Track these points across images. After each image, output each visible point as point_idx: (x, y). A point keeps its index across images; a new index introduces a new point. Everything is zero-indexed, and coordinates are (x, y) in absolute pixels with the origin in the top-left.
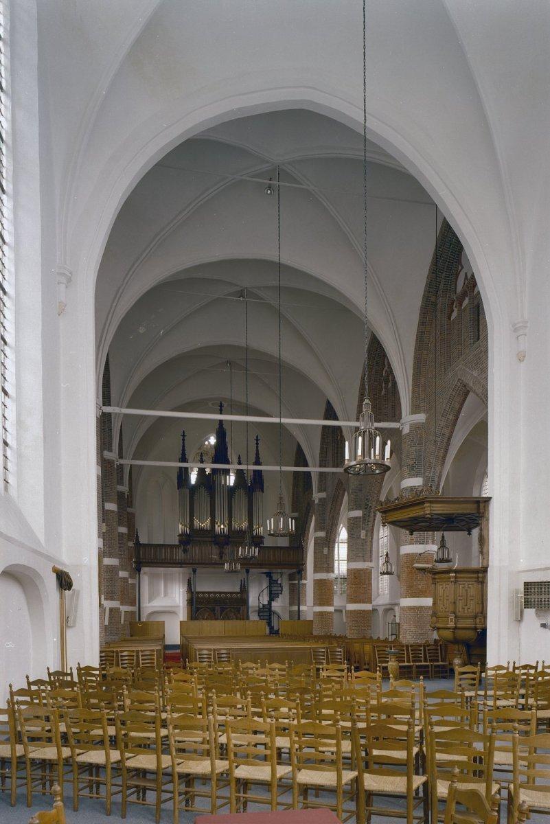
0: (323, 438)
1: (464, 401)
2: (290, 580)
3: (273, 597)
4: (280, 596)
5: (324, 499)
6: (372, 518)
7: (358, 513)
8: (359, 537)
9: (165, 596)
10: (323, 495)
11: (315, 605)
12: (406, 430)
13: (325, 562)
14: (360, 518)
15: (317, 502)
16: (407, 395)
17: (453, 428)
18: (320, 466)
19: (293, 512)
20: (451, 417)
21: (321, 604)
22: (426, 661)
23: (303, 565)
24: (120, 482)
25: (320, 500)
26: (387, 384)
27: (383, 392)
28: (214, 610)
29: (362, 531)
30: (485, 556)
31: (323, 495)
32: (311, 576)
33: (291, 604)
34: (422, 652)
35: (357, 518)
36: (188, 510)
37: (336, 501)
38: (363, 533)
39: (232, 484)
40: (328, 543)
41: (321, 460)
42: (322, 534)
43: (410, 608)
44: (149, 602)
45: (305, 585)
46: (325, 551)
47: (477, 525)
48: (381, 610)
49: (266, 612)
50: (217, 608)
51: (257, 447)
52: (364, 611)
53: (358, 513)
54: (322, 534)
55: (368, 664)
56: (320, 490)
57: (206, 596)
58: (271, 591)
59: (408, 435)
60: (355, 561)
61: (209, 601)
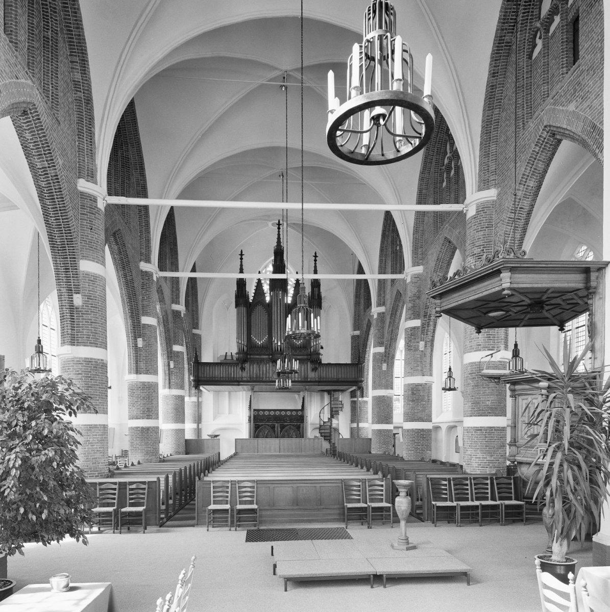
0: (382, 250)
1: (551, 159)
2: (352, 397)
3: (334, 413)
4: (340, 413)
5: (383, 313)
6: (431, 328)
7: (417, 323)
8: (417, 349)
9: (229, 413)
10: (382, 309)
11: (373, 423)
12: (471, 212)
13: (385, 381)
14: (418, 328)
15: (375, 316)
16: (473, 170)
17: (534, 200)
18: (380, 273)
19: (355, 330)
20: (532, 183)
21: (380, 421)
22: (493, 499)
23: (362, 381)
24: (176, 300)
25: (379, 314)
26: (449, 172)
27: (444, 184)
28: (274, 427)
29: (421, 342)
30: (598, 355)
31: (382, 309)
32: (371, 393)
33: (352, 421)
34: (489, 487)
35: (414, 328)
36: (245, 329)
37: (395, 313)
38: (422, 344)
39: (289, 302)
40: (388, 358)
41: (380, 267)
42: (381, 350)
43: (479, 429)
44: (215, 418)
45: (366, 402)
46: (384, 367)
47: (586, 308)
48: (444, 427)
49: (327, 432)
50: (276, 425)
51: (315, 264)
52: (423, 430)
53: (417, 323)
54: (381, 350)
55: (421, 500)
56: (379, 304)
57: (267, 413)
58: (331, 408)
59: (474, 217)
60: (412, 375)
61: (269, 418)
